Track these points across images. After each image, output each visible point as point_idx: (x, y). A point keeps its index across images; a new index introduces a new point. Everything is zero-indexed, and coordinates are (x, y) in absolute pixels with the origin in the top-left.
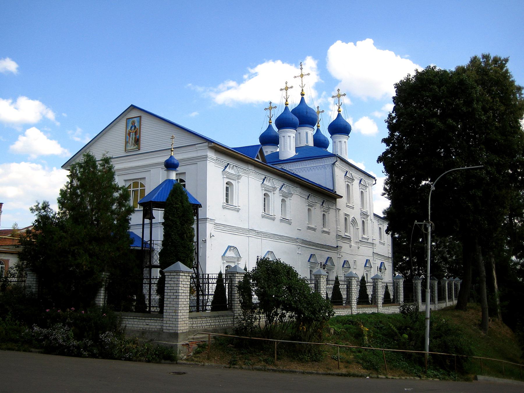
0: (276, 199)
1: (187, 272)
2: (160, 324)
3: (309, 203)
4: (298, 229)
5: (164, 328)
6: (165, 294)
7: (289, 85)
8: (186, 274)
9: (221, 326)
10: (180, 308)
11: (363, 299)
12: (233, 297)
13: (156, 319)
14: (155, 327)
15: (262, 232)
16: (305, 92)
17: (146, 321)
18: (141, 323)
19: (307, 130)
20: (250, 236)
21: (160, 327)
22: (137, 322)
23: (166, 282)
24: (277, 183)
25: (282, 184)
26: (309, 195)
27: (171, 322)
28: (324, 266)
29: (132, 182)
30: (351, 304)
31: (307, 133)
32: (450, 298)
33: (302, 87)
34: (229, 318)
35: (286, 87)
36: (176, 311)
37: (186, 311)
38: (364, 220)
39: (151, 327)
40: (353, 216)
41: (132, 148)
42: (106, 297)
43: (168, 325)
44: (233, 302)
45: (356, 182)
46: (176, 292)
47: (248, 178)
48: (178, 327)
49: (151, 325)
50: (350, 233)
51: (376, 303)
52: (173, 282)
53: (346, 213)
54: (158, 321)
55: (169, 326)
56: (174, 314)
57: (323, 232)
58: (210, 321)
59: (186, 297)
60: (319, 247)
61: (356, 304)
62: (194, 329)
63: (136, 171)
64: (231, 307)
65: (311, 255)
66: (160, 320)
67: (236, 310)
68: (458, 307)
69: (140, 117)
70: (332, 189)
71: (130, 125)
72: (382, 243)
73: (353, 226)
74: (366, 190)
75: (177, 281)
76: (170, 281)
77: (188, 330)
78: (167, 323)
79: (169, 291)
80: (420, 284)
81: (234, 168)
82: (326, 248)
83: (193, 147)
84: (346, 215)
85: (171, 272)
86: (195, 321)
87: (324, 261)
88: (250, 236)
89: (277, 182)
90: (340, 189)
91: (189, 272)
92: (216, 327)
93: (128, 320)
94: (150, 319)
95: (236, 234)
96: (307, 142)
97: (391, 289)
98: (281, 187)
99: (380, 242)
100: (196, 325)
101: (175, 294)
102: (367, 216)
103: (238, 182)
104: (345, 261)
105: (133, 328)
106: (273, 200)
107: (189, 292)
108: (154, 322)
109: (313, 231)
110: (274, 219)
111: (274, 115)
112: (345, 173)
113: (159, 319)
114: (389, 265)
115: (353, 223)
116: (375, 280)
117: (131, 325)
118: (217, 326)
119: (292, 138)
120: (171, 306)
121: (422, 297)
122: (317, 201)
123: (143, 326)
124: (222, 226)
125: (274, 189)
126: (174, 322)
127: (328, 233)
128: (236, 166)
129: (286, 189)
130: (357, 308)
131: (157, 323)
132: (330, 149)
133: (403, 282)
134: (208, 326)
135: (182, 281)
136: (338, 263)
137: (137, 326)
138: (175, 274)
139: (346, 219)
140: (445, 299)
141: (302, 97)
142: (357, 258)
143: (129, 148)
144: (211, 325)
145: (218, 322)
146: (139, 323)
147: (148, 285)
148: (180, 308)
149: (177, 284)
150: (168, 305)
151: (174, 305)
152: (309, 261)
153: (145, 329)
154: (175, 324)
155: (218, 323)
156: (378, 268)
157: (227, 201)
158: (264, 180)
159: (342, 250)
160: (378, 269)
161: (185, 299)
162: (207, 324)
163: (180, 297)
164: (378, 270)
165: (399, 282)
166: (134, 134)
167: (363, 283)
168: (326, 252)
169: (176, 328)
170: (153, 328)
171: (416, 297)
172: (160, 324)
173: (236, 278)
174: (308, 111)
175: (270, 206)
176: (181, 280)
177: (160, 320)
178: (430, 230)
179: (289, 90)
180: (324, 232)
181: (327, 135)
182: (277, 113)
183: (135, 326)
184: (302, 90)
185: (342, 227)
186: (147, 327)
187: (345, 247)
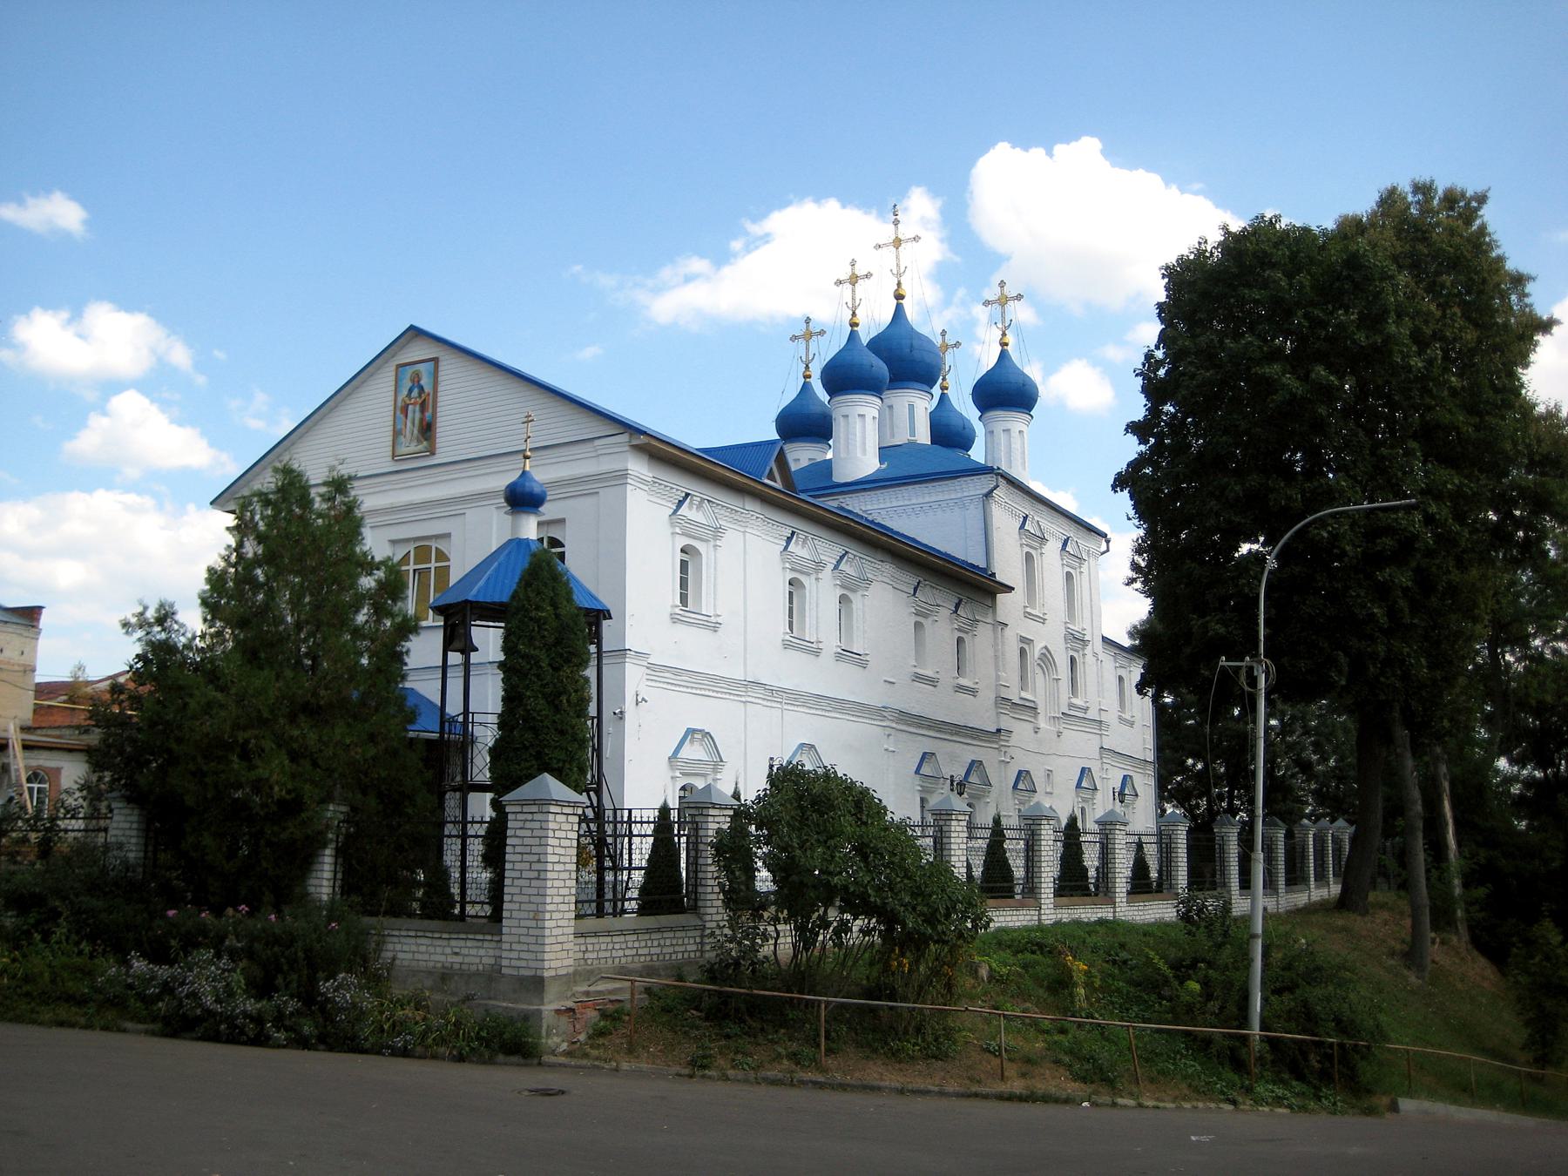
0: (823, 594)
2: (491, 952)
9: (617, 960)
11: (1073, 881)
13: (480, 937)
16: (906, 289)
17: (453, 943)
18: (439, 950)
19: (912, 399)
21: (492, 961)
22: (428, 946)
23: (509, 833)
25: (839, 551)
26: (918, 583)
27: (525, 947)
28: (960, 787)
29: (411, 547)
30: (1038, 896)
31: (911, 407)
33: (899, 275)
34: (689, 934)
35: (853, 274)
36: (538, 916)
38: (1075, 655)
40: (1043, 645)
41: (413, 448)
44: (700, 889)
45: (1053, 546)
46: (539, 861)
47: (745, 536)
52: (528, 833)
53: (1023, 635)
54: (486, 944)
55: (519, 959)
56: (533, 923)
59: (565, 876)
60: (945, 733)
62: (589, 968)
63: (423, 514)
69: (436, 360)
70: (983, 565)
71: (407, 384)
72: (1125, 720)
78: (511, 950)
79: (518, 857)
82: (966, 736)
84: (1023, 640)
85: (523, 803)
87: (959, 773)
90: (1007, 567)
92: (652, 960)
93: (403, 940)
95: (711, 694)
96: (913, 433)
97: (1151, 851)
104: (1020, 772)
108: (477, 947)
110: (817, 653)
111: (817, 354)
112: (1022, 520)
113: (489, 937)
114: (1145, 785)
118: (655, 958)
119: (868, 419)
120: (525, 899)
122: (941, 600)
123: (443, 958)
124: (668, 672)
125: (819, 566)
126: (532, 948)
130: (1056, 907)
132: (977, 453)
133: (1185, 833)
134: (630, 959)
135: (554, 830)
136: (1002, 779)
137: (426, 957)
138: (534, 809)
139: (1023, 652)
140: (1305, 880)
142: (1054, 764)
143: (402, 450)
144: (637, 955)
145: (659, 945)
147: (459, 841)
149: (540, 838)
152: (917, 772)
155: (658, 950)
157: (684, 599)
158: (789, 540)
159: (1014, 740)
162: (628, 952)
166: (418, 408)
167: (1071, 835)
168: (965, 746)
171: (1302, 869)
172: (491, 952)
174: (915, 343)
180: (960, 688)
181: (970, 412)
183: (417, 956)
184: (899, 284)
185: (1011, 675)
187: (1021, 732)
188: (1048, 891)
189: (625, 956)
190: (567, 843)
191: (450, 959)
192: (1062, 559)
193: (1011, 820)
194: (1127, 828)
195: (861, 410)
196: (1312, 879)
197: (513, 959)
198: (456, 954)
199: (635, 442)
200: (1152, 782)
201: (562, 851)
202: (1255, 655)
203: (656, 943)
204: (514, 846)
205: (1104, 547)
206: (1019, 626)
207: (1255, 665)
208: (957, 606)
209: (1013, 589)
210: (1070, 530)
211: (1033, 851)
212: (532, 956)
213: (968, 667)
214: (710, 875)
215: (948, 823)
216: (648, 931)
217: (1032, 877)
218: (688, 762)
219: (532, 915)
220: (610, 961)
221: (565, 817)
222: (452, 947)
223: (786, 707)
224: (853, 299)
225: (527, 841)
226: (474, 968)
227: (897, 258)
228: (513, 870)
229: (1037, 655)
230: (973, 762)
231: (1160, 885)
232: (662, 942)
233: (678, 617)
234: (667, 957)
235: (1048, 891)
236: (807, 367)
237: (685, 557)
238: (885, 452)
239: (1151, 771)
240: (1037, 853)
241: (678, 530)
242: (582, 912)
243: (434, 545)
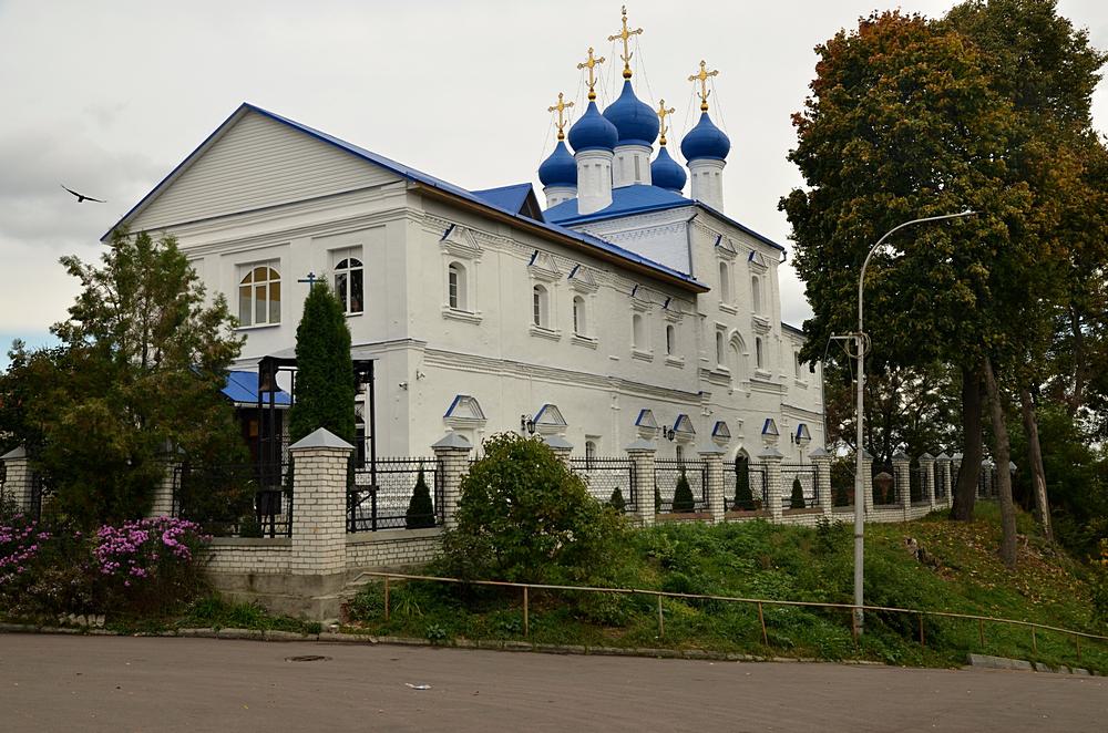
0: (560, 296)
1: (339, 450)
5: (294, 566)
8: (336, 454)
9: (381, 563)
11: (744, 499)
15: (531, 366)
17: (258, 553)
18: (248, 559)
21: (286, 565)
25: (573, 264)
27: (308, 555)
28: (670, 434)
29: (252, 269)
31: (636, 158)
32: (940, 494)
33: (627, 59)
37: (340, 530)
38: (760, 337)
39: (268, 565)
40: (735, 329)
42: (177, 508)
43: (301, 560)
52: (309, 471)
54: (282, 553)
56: (313, 537)
58: (396, 550)
59: (338, 501)
65: (643, 411)
68: (952, 515)
70: (687, 273)
72: (800, 384)
77: (344, 570)
79: (302, 489)
82: (676, 397)
83: (376, 192)
84: (719, 326)
85: (304, 450)
87: (671, 424)
91: (344, 450)
96: (638, 178)
97: (429, 479)
98: (573, 272)
100: (364, 559)
101: (314, 495)
102: (767, 328)
104: (718, 423)
105: (230, 570)
107: (345, 490)
110: (557, 339)
117: (227, 564)
118: (411, 560)
119: (603, 168)
120: (308, 519)
122: (656, 300)
123: (251, 565)
125: (558, 275)
127: (680, 365)
132: (687, 193)
134: (391, 561)
136: (704, 429)
137: (239, 565)
138: (312, 454)
139: (719, 335)
140: (928, 497)
141: (626, 82)
146: (243, 559)
147: (370, 476)
150: (301, 519)
152: (637, 424)
155: (413, 554)
157: (453, 302)
158: (534, 257)
159: (712, 400)
162: (389, 556)
167: (742, 464)
172: (285, 559)
174: (638, 110)
178: (861, 352)
180: (670, 363)
181: (681, 160)
182: (574, 115)
183: (234, 564)
184: (627, 66)
185: (709, 352)
187: (717, 393)
190: (339, 478)
194: (783, 461)
196: (933, 497)
198: (261, 561)
199: (410, 188)
200: (822, 428)
201: (335, 484)
202: (856, 330)
203: (412, 549)
205: (782, 258)
207: (856, 338)
208: (667, 304)
209: (708, 289)
210: (755, 246)
213: (676, 346)
214: (452, 499)
218: (459, 420)
219: (313, 531)
220: (376, 563)
224: (591, 79)
225: (308, 477)
229: (730, 337)
230: (681, 416)
232: (417, 548)
234: (421, 559)
237: (453, 271)
238: (617, 193)
239: (821, 421)
243: (268, 266)
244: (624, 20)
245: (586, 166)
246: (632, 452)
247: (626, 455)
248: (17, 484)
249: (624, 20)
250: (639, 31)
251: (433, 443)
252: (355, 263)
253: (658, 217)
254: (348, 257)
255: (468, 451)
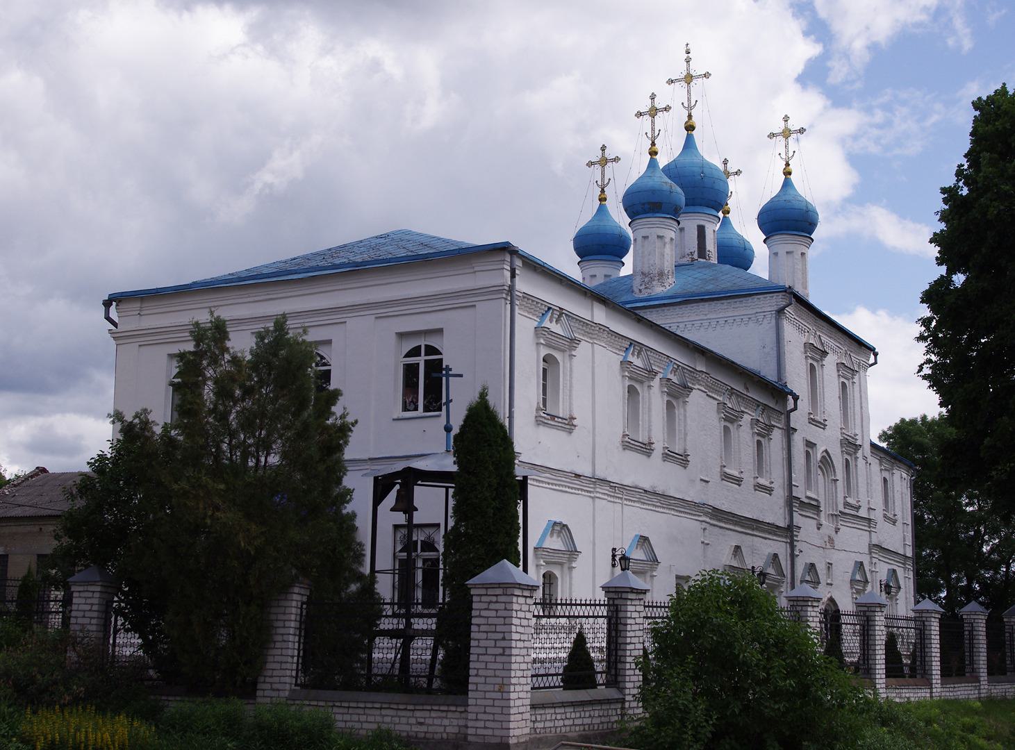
2: (455, 722)
3: (726, 411)
4: (701, 480)
5: (470, 731)
6: (471, 645)
7: (659, 104)
9: (558, 730)
10: (513, 681)
12: (620, 653)
13: (445, 708)
14: (442, 731)
17: (418, 714)
20: (598, 495)
21: (456, 730)
22: (392, 717)
23: (474, 613)
24: (656, 360)
27: (491, 717)
30: (873, 676)
31: (701, 231)
33: (690, 108)
34: (613, 707)
35: (653, 106)
36: (503, 688)
38: (849, 458)
39: (431, 729)
40: (823, 448)
43: (481, 724)
44: (620, 666)
45: (831, 361)
46: (504, 639)
47: (593, 347)
48: (509, 729)
49: (431, 725)
50: (818, 495)
51: (927, 674)
52: (493, 614)
54: (450, 715)
55: (485, 728)
56: (498, 695)
57: (757, 488)
61: (884, 676)
62: (538, 736)
64: (616, 679)
66: (456, 711)
67: (95, 615)
72: (889, 519)
73: (824, 474)
74: (854, 380)
75: (506, 609)
76: (485, 609)
78: (477, 720)
80: (982, 625)
81: (562, 318)
85: (487, 586)
86: (541, 714)
88: (598, 495)
89: (657, 357)
90: (797, 380)
91: (937, 612)
92: (584, 730)
93: (367, 711)
94: (395, 709)
95: (567, 489)
99: (885, 516)
102: (857, 447)
103: (569, 356)
106: (647, 404)
108: (440, 718)
109: (735, 485)
111: (612, 179)
113: (453, 708)
114: (906, 579)
115: (824, 465)
116: (865, 615)
121: (941, 661)
123: (407, 728)
126: (497, 717)
128: (566, 315)
129: (675, 375)
131: (447, 718)
133: (984, 621)
134: (568, 728)
135: (516, 611)
138: (499, 591)
139: (808, 454)
142: (835, 557)
144: (573, 725)
145: (590, 716)
146: (397, 720)
148: (513, 681)
149: (505, 618)
151: (498, 673)
153: (415, 735)
154: (502, 722)
156: (881, 585)
160: (881, 587)
161: (523, 656)
162: (567, 722)
163: (514, 652)
164: (881, 591)
165: (976, 621)
168: (764, 540)
169: (503, 733)
170: (437, 733)
171: (972, 662)
172: (455, 722)
173: (629, 603)
174: (706, 170)
175: (641, 418)
176: (515, 607)
177: (456, 711)
179: (660, 118)
180: (759, 487)
184: (690, 116)
186: (417, 730)
188: (881, 672)
189: (564, 726)
191: (415, 729)
192: (838, 371)
193: (846, 604)
195: (661, 232)
197: (479, 729)
198: (421, 724)
204: (479, 625)
205: (872, 360)
206: (804, 430)
211: (868, 635)
212: (498, 725)
215: (804, 608)
216: (573, 704)
217: (868, 660)
219: (497, 688)
220: (553, 730)
221: (524, 599)
222: (416, 718)
223: (625, 502)
224: (653, 130)
226: (438, 737)
227: (689, 92)
228: (478, 646)
229: (819, 457)
231: (913, 669)
232: (592, 713)
233: (543, 420)
235: (881, 672)
236: (603, 191)
240: (872, 637)
241: (542, 341)
242: (536, 685)
244: (688, 61)
245: (645, 238)
246: (607, 589)
247: (601, 596)
248: (87, 614)
249: (688, 61)
250: (707, 75)
251: (601, 585)
252: (431, 350)
253: (738, 305)
254: (422, 342)
255: (645, 593)
